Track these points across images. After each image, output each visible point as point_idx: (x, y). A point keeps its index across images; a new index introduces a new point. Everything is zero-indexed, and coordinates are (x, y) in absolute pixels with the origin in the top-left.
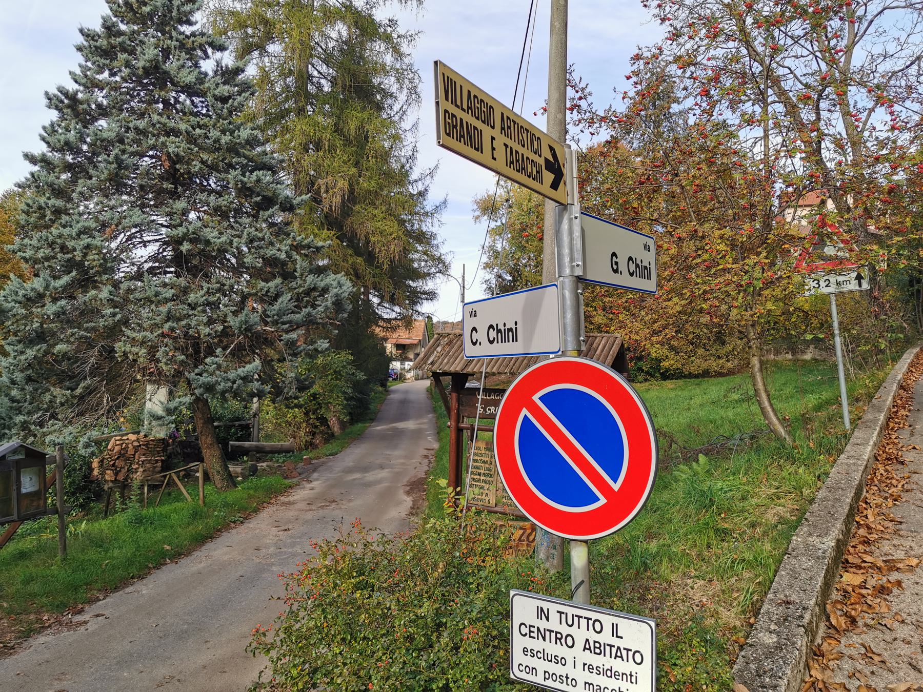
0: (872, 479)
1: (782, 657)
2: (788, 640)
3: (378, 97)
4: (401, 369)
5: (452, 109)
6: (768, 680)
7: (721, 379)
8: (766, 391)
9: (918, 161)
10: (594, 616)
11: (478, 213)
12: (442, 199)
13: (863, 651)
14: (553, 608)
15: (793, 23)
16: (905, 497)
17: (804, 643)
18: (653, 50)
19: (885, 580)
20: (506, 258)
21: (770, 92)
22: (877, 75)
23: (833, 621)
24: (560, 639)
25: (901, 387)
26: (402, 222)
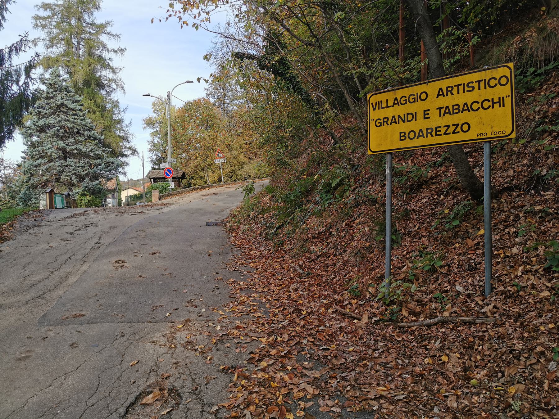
11: (145, 125)
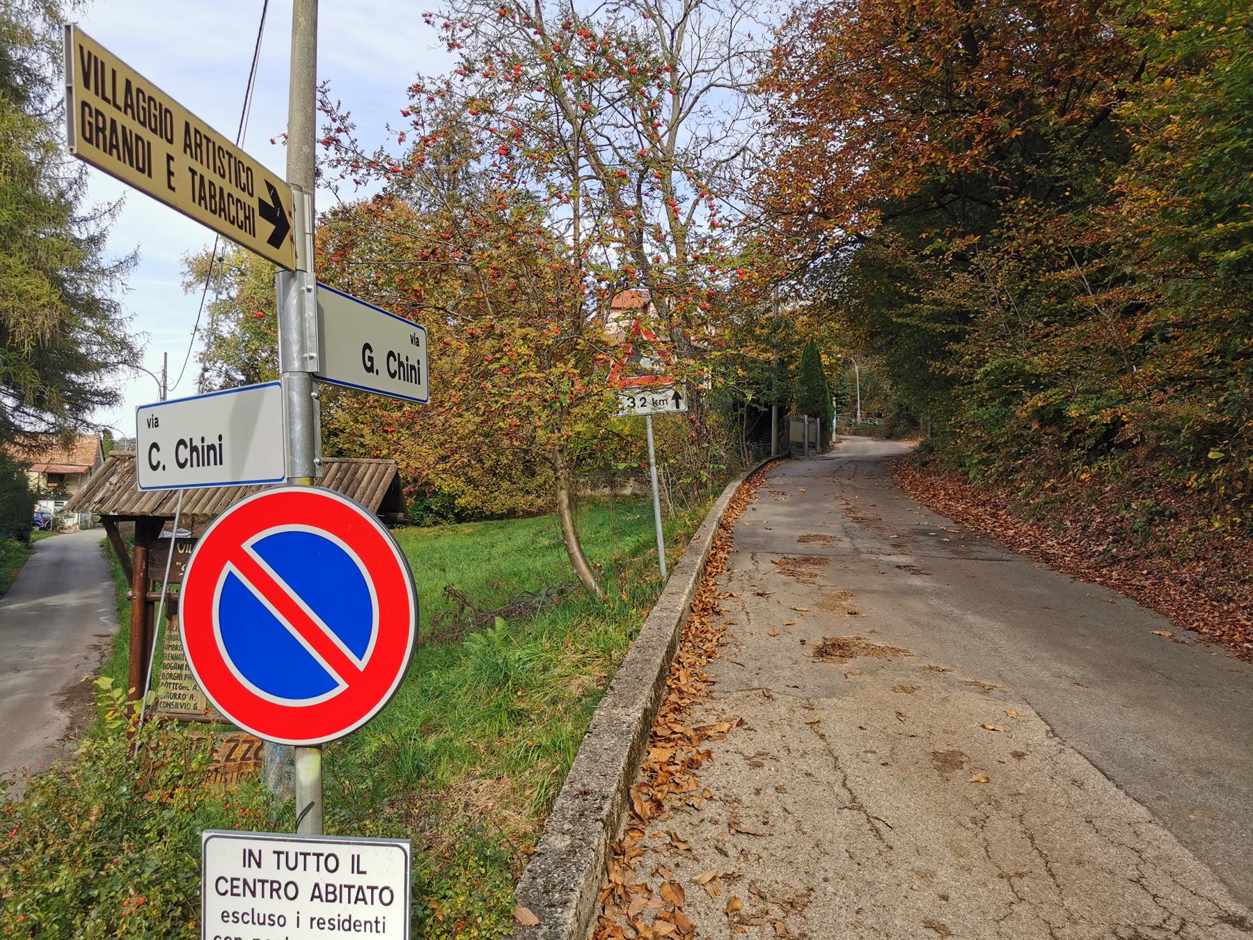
0: (686, 634)
1: (575, 864)
2: (583, 840)
3: (18, 79)
5: (96, 102)
6: (557, 895)
7: (530, 520)
8: (575, 533)
9: (736, 265)
10: (325, 849)
11: (189, 278)
12: (130, 252)
13: (668, 840)
14: (266, 848)
15: (606, 82)
16: (720, 652)
17: (602, 842)
18: (438, 83)
19: (694, 751)
20: (236, 348)
21: (582, 161)
22: (702, 162)
23: (637, 809)
24: (277, 891)
25: (722, 526)
26: (58, 282)
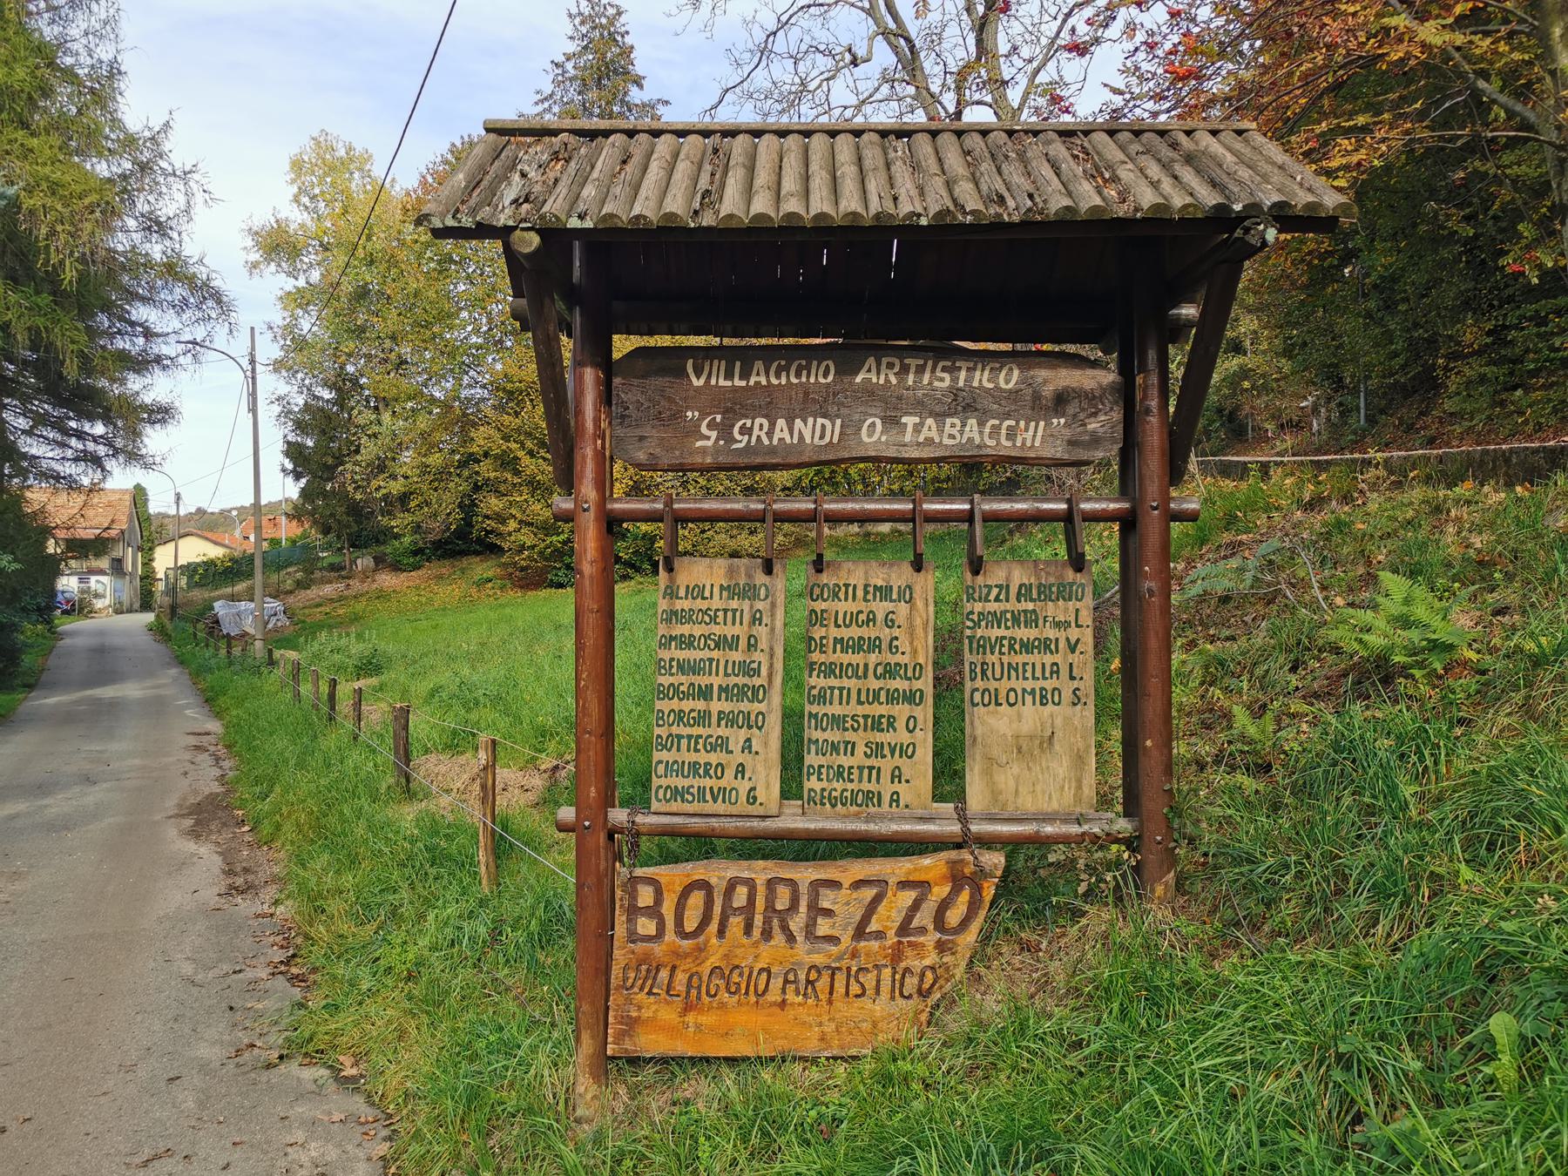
4: (82, 592)
